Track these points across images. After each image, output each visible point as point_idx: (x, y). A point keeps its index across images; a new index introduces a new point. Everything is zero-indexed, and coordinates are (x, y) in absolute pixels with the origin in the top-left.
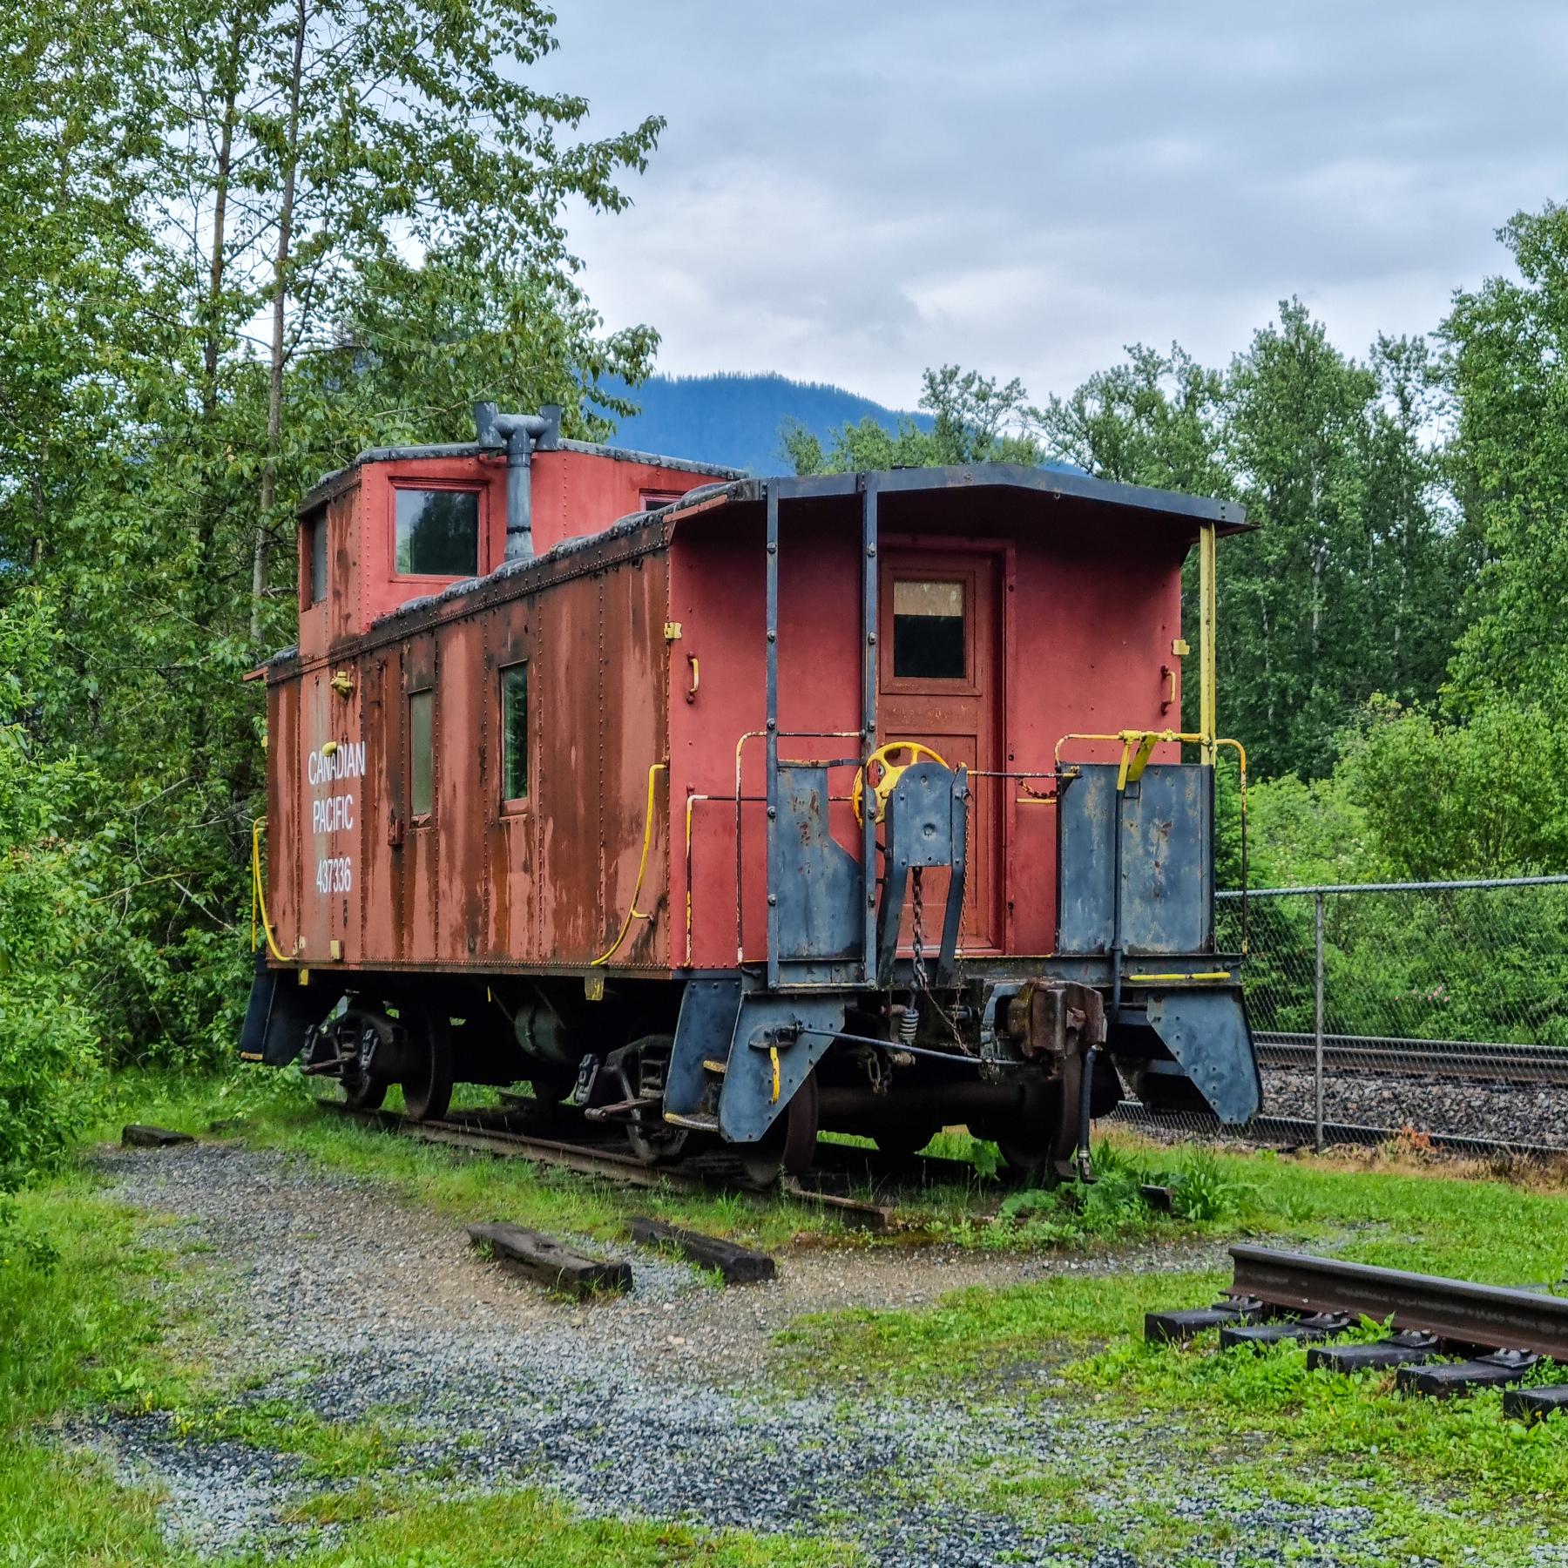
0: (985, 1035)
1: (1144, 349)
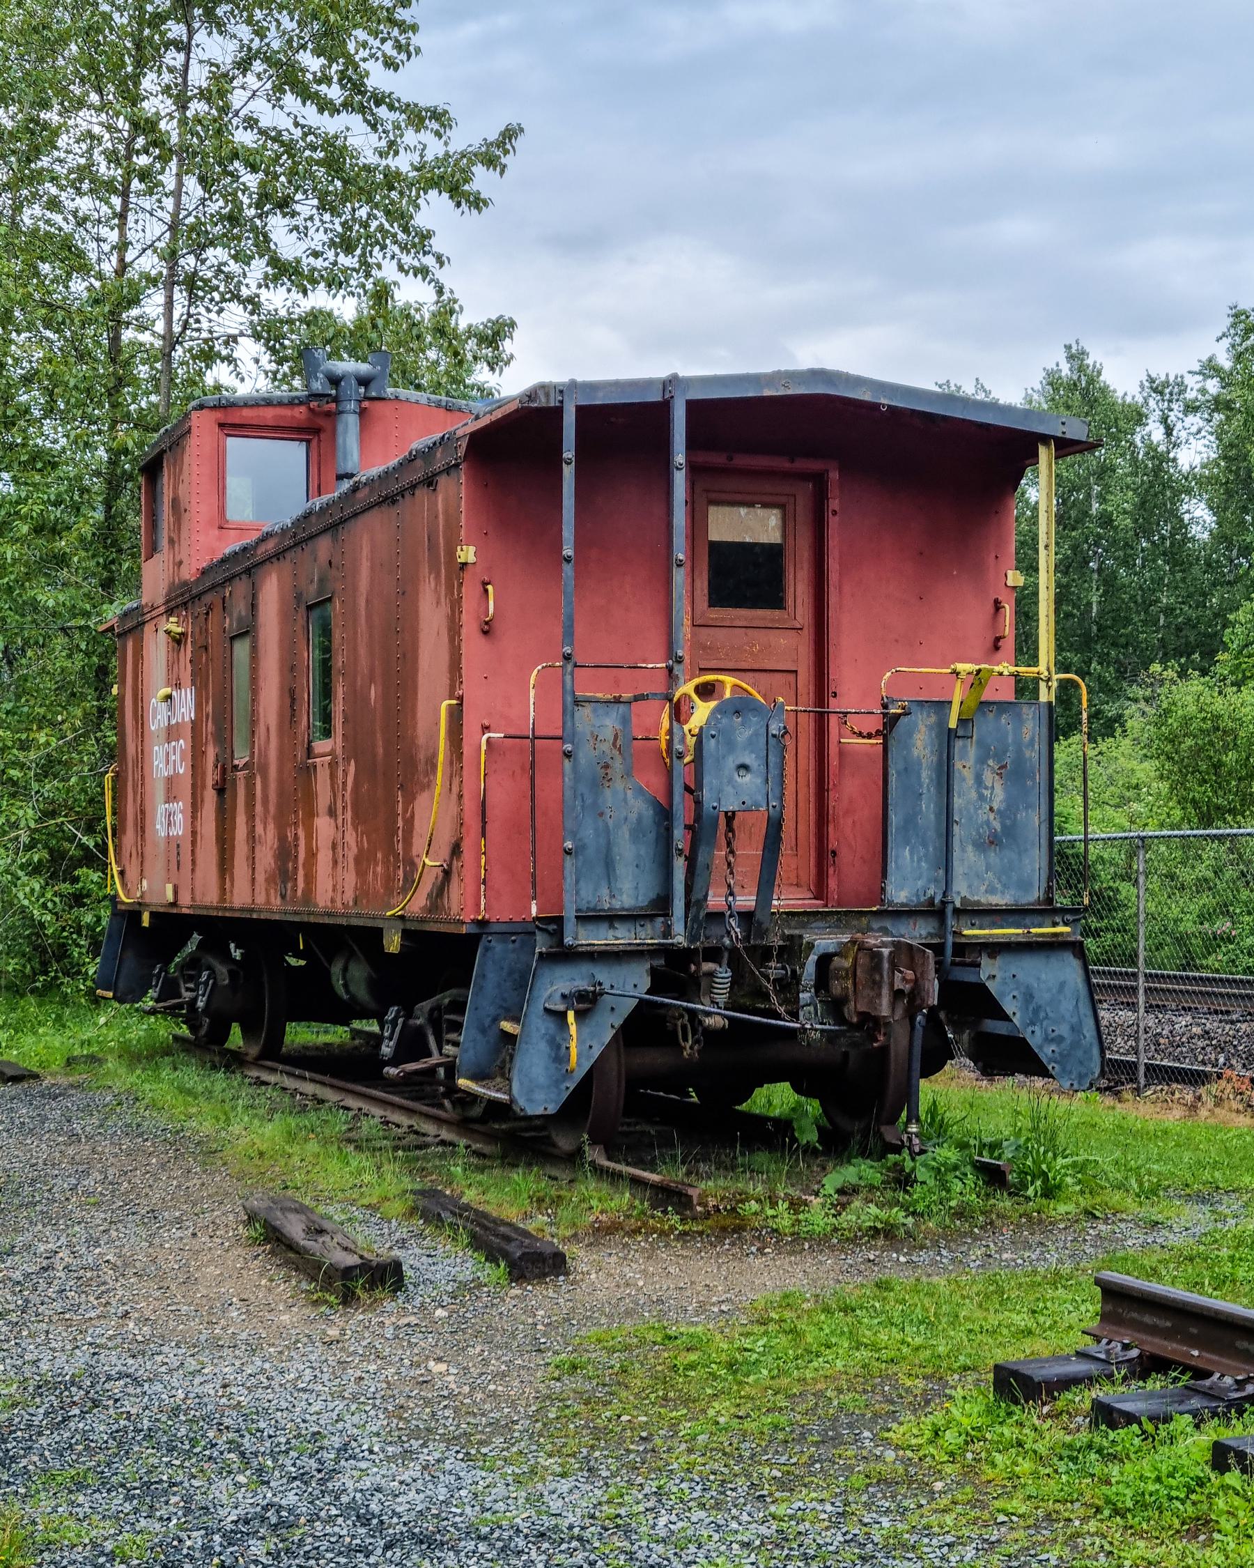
0: (805, 997)
1: (952, 385)
